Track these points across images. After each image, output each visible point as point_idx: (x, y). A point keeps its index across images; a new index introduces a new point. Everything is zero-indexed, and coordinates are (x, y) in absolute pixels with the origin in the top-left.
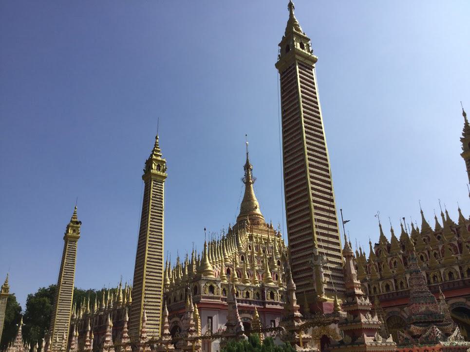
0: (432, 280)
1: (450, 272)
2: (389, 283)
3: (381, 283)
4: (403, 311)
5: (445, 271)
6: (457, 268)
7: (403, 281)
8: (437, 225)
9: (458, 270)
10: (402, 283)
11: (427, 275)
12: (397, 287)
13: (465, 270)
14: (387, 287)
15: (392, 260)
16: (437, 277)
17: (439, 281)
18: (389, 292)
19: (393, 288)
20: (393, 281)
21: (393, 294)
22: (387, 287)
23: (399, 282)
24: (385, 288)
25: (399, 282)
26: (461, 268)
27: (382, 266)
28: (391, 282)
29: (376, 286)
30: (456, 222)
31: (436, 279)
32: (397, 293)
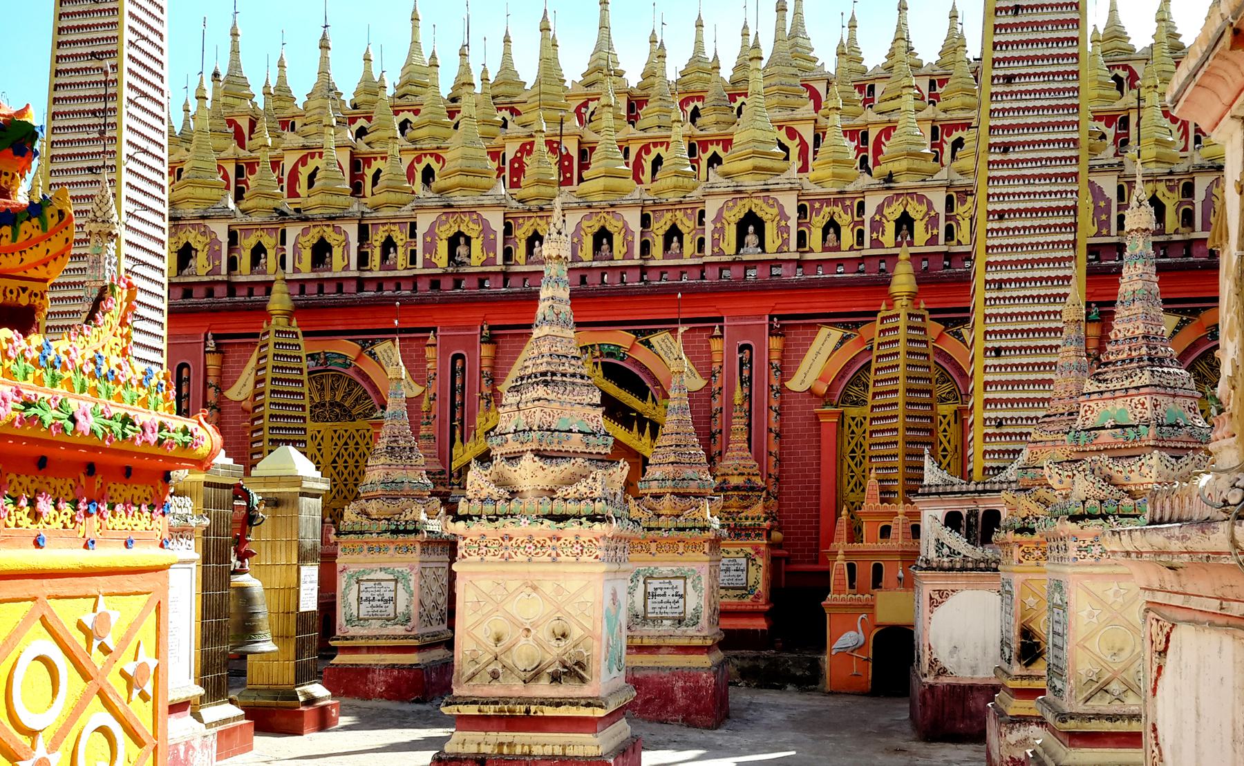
0: (520, 252)
1: (603, 228)
2: (331, 237)
3: (293, 232)
4: (373, 355)
5: (585, 224)
6: (633, 219)
7: (400, 237)
8: (954, 44)
9: (635, 226)
10: (389, 244)
11: (508, 230)
12: (363, 259)
13: (444, 236)
14: (321, 251)
15: (303, 161)
16: (468, 241)
17: (399, 267)
18: (327, 275)
19: (342, 263)
20: (352, 230)
21: (339, 283)
22: (321, 251)
23: (377, 238)
24: (307, 255)
25: (377, 238)
26: (645, 221)
27: (369, 173)
28: (781, 207)
29: (269, 241)
30: (828, 60)
31: (392, 256)
32: (232, 288)
